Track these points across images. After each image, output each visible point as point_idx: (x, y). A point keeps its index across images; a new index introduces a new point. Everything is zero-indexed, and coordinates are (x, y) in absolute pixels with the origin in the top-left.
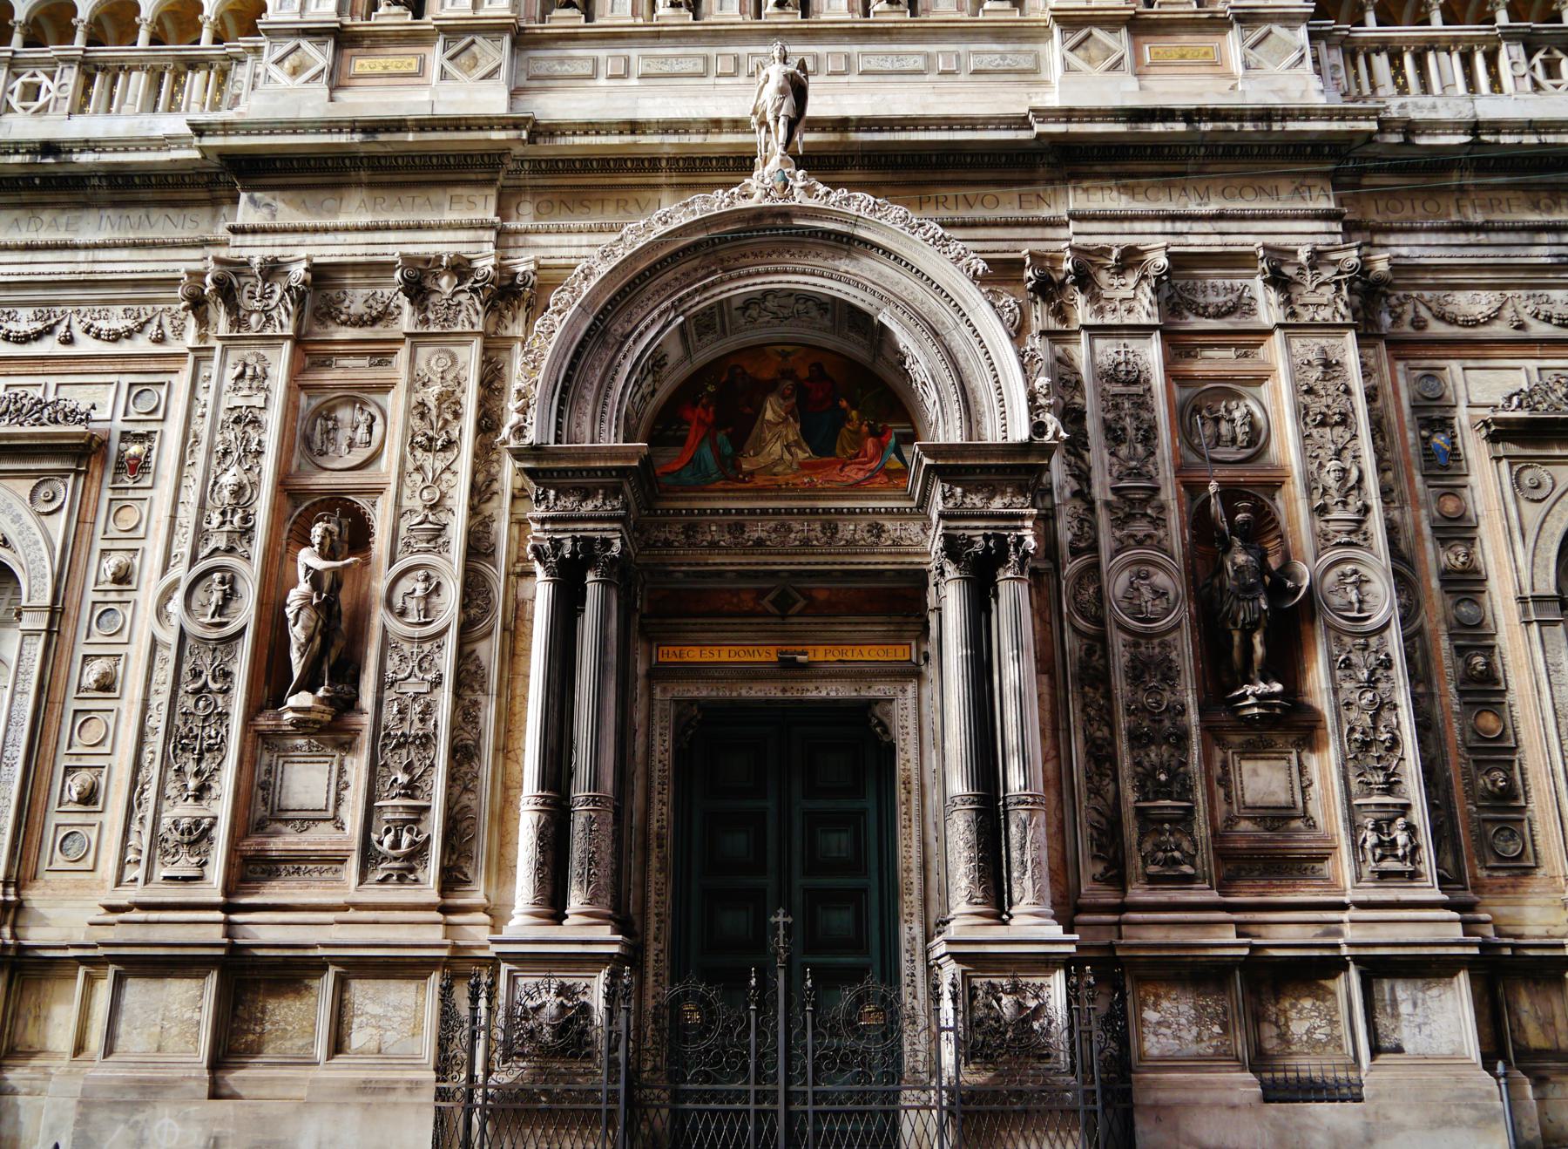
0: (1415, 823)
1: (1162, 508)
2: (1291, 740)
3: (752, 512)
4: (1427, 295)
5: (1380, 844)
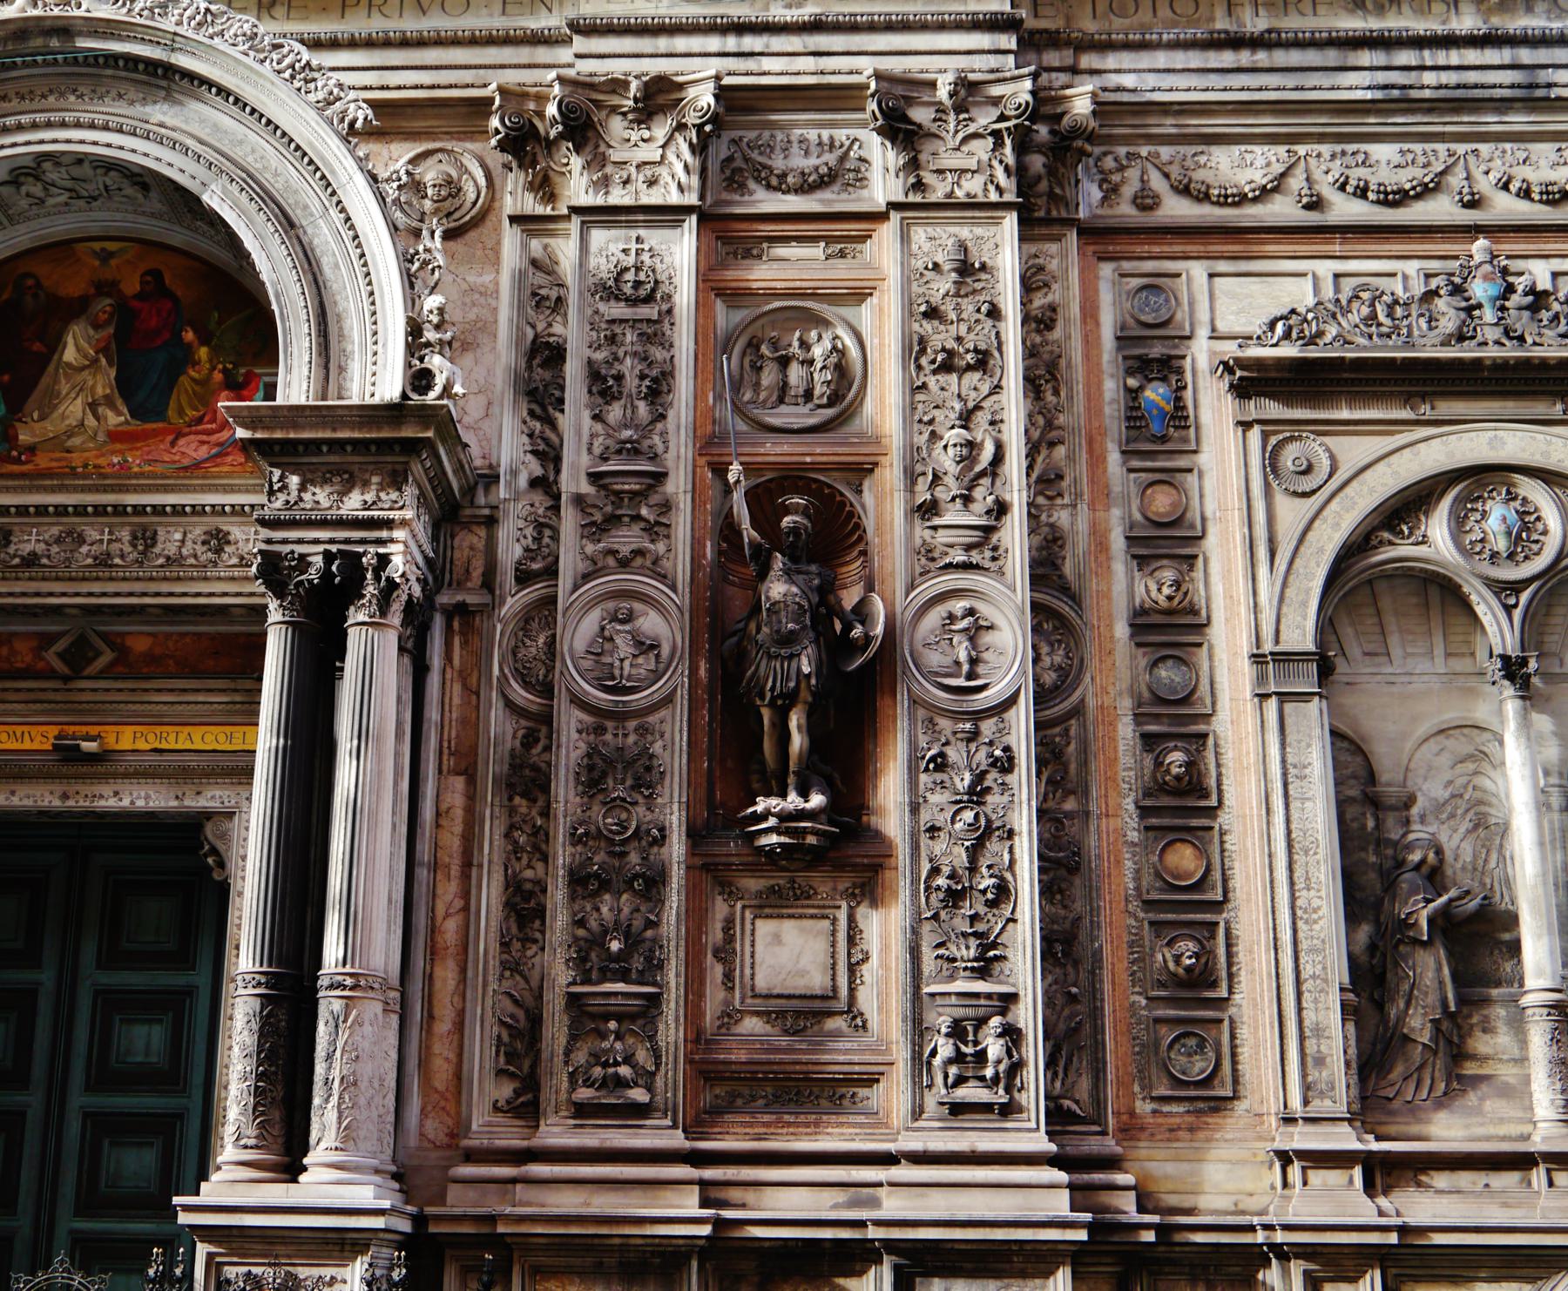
0: (1021, 1025)
1: (666, 506)
2: (841, 887)
3: (22, 510)
4: (1166, 152)
5: (959, 1058)
